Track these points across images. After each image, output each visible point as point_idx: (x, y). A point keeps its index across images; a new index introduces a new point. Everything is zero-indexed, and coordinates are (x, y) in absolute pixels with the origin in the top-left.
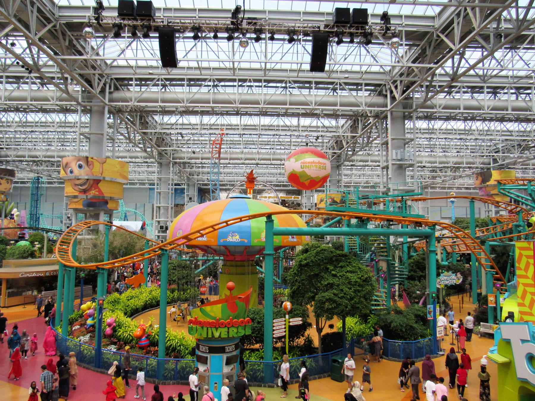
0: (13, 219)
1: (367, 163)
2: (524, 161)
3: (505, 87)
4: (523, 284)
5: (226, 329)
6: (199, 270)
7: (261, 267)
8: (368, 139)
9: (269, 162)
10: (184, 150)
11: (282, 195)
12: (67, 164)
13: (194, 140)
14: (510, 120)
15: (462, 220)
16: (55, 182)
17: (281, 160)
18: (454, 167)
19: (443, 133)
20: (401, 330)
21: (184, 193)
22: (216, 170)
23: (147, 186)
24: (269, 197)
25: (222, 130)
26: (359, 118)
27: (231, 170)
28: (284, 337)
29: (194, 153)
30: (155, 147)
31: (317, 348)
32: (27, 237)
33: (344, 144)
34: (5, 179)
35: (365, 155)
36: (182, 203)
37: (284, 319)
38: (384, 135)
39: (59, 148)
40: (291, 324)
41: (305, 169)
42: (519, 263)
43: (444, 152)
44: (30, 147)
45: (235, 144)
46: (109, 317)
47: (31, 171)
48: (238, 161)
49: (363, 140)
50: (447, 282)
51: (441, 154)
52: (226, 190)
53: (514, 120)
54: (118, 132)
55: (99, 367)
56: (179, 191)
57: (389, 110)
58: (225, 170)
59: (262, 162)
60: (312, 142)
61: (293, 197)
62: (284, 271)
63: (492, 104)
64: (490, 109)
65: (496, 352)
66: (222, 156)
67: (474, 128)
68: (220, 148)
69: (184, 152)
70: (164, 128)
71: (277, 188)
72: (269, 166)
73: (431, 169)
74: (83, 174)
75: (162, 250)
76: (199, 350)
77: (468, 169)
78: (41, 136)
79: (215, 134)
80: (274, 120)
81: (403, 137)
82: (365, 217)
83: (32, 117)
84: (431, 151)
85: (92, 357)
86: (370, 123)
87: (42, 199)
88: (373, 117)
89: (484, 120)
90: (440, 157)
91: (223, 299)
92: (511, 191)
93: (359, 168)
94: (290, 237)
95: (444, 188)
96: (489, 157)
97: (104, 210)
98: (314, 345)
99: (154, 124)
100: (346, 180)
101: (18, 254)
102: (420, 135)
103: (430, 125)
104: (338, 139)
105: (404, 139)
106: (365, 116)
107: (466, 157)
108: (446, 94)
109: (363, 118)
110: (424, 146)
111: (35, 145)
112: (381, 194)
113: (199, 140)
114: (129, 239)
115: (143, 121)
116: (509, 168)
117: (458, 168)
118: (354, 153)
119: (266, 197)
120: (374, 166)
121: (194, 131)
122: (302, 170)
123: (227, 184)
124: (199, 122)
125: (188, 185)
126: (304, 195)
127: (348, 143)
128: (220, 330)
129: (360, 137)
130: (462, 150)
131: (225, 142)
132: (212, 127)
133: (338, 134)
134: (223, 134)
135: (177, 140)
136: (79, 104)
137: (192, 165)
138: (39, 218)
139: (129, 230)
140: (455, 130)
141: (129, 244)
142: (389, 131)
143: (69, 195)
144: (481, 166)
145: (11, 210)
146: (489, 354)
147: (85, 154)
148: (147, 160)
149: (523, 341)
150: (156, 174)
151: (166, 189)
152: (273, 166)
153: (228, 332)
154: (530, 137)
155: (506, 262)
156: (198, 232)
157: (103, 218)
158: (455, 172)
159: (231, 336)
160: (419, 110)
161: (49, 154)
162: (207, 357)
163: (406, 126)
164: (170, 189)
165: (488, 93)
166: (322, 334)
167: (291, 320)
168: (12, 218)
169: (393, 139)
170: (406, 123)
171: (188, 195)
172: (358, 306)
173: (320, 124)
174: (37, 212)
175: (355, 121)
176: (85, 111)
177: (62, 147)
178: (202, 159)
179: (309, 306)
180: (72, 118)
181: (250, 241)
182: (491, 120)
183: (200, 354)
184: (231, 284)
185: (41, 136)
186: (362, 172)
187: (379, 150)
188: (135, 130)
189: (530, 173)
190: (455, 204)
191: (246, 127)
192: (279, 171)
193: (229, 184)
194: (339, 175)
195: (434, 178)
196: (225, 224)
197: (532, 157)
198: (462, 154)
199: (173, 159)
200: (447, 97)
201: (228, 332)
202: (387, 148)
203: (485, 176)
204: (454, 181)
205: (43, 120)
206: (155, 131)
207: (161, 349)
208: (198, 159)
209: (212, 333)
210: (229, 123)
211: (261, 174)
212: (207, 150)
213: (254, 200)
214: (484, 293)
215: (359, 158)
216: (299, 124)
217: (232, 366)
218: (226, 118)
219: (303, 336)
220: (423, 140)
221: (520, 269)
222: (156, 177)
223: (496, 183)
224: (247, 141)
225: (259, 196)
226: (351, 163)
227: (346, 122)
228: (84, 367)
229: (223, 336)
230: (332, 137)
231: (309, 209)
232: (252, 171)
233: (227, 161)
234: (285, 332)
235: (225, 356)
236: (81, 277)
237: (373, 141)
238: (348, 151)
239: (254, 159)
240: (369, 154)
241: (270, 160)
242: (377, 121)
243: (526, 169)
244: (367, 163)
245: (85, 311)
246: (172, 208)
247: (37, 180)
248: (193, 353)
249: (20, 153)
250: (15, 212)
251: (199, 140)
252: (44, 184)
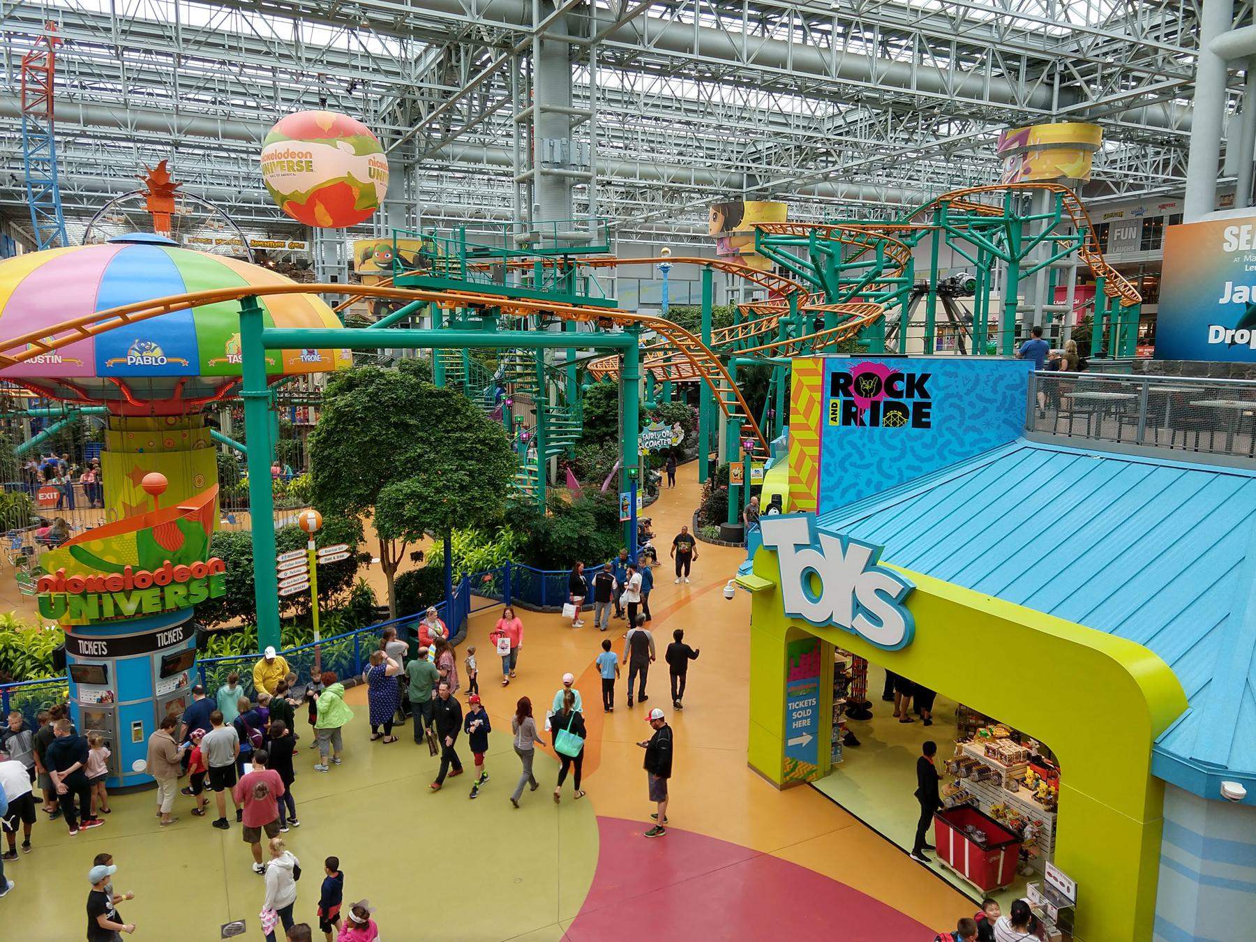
2: (806, 184)
3: (785, 9)
4: (800, 441)
5: (157, 591)
6: (24, 446)
8: (483, 106)
9: (212, 141)
11: (253, 236)
14: (786, 90)
17: (249, 139)
18: (671, 188)
20: (570, 548)
24: (219, 242)
25: (51, 25)
26: (461, 44)
27: (89, 155)
28: (307, 593)
31: (385, 608)
35: (473, 146)
37: (304, 552)
38: (524, 96)
40: (322, 561)
42: (796, 403)
43: (653, 150)
45: (100, 76)
49: (470, 106)
50: (655, 444)
51: (645, 156)
52: (79, 214)
53: (758, 86)
57: (537, 33)
58: (69, 153)
60: (336, 97)
61: (287, 242)
62: (281, 437)
63: (756, 47)
64: (654, 42)
65: (750, 572)
67: (716, 99)
68: (51, 84)
71: (239, 217)
72: (214, 153)
73: (623, 189)
79: (25, 36)
80: (222, 15)
81: (567, 109)
84: (626, 148)
86: (489, 60)
88: (496, 46)
89: (737, 84)
92: (780, 249)
93: (457, 175)
94: (305, 351)
95: (648, 236)
96: (740, 171)
98: (376, 602)
100: (426, 206)
102: (604, 107)
103: (626, 80)
104: (407, 96)
105: (570, 114)
106: (472, 38)
107: (698, 166)
108: (663, 9)
112: (515, 248)
116: (776, 198)
117: (678, 191)
119: (209, 241)
122: (368, 180)
123: (81, 198)
126: (319, 240)
127: (432, 107)
128: (136, 596)
129: (463, 95)
131: (64, 67)
133: (407, 82)
144: (725, 189)
146: (739, 577)
149: (798, 547)
152: (225, 154)
154: (820, 132)
155: (763, 398)
156: (33, 339)
158: (672, 199)
160: (604, 42)
162: (105, 667)
165: (751, 19)
166: (396, 575)
167: (322, 552)
170: (574, 70)
173: (355, 46)
179: (361, 517)
181: (195, 363)
182: (751, 85)
183: (80, 661)
184: (154, 477)
186: (466, 187)
187: (508, 135)
189: (813, 211)
193: (89, 198)
194: (410, 190)
195: (628, 211)
197: (820, 176)
198: (687, 159)
200: (667, 17)
201: (162, 598)
202: (531, 131)
203: (731, 213)
209: (116, 605)
211: (190, 174)
213: (257, 266)
214: (721, 462)
215: (459, 150)
217: (180, 677)
219: (349, 584)
220: (609, 117)
221: (797, 412)
223: (753, 229)
224: (140, 71)
226: (439, 162)
227: (425, 51)
229: (147, 608)
230: (389, 89)
231: (334, 279)
232: (163, 164)
234: (309, 580)
235: (157, 657)
237: (494, 109)
239: (165, 129)
240: (483, 144)
243: (806, 201)
248: (58, 660)
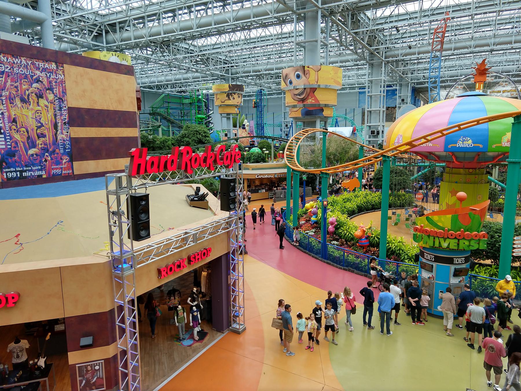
7: (491, 175)
9: (509, 46)
10: (397, 46)
12: (286, 76)
13: (411, 32)
16: (274, 93)
21: (396, 94)
22: (437, 65)
23: (357, 90)
25: (447, 13)
29: (410, 47)
30: (366, 47)
32: (256, 144)
34: (237, 94)
36: (394, 106)
39: (276, 60)
44: (254, 62)
46: (332, 217)
47: (256, 84)
48: (466, 50)
52: (445, 87)
55: (325, 259)
56: (391, 93)
58: (446, 63)
66: (445, 46)
68: (443, 37)
69: (398, 49)
71: (516, 79)
72: (508, 51)
74: (300, 84)
75: (384, 156)
76: (423, 256)
78: (262, 51)
79: (437, 20)
83: (254, 33)
85: (319, 249)
87: (265, 109)
99: (367, 21)
101: (254, 159)
111: (257, 60)
113: (416, 31)
114: (344, 145)
115: (355, 20)
119: (499, 92)
125: (401, 85)
128: (448, 241)
134: (448, 19)
135: (391, 35)
136: (294, 12)
139: (343, 136)
141: (343, 149)
145: (243, 121)
147: (302, 63)
148: (358, 62)
150: (366, 77)
151: (378, 91)
152: (514, 51)
153: (458, 244)
157: (319, 125)
159: (461, 247)
161: (269, 67)
164: (382, 92)
171: (400, 97)
174: (261, 122)
176: (299, 20)
178: (419, 54)
180: (288, 28)
184: (461, 194)
185: (262, 51)
188: (346, 31)
193: (450, 80)
196: (457, 128)
199: (386, 58)
201: (458, 244)
205: (263, 34)
206: (367, 29)
207: (382, 252)
208: (414, 54)
209: (440, 243)
210: (457, 3)
211: (495, 63)
217: (461, 278)
222: (367, 79)
228: (313, 257)
229: (451, 247)
232: (484, 60)
233: (450, 52)
235: (453, 268)
241: (510, 43)
248: (416, 258)
250: (246, 122)
251: (416, 31)
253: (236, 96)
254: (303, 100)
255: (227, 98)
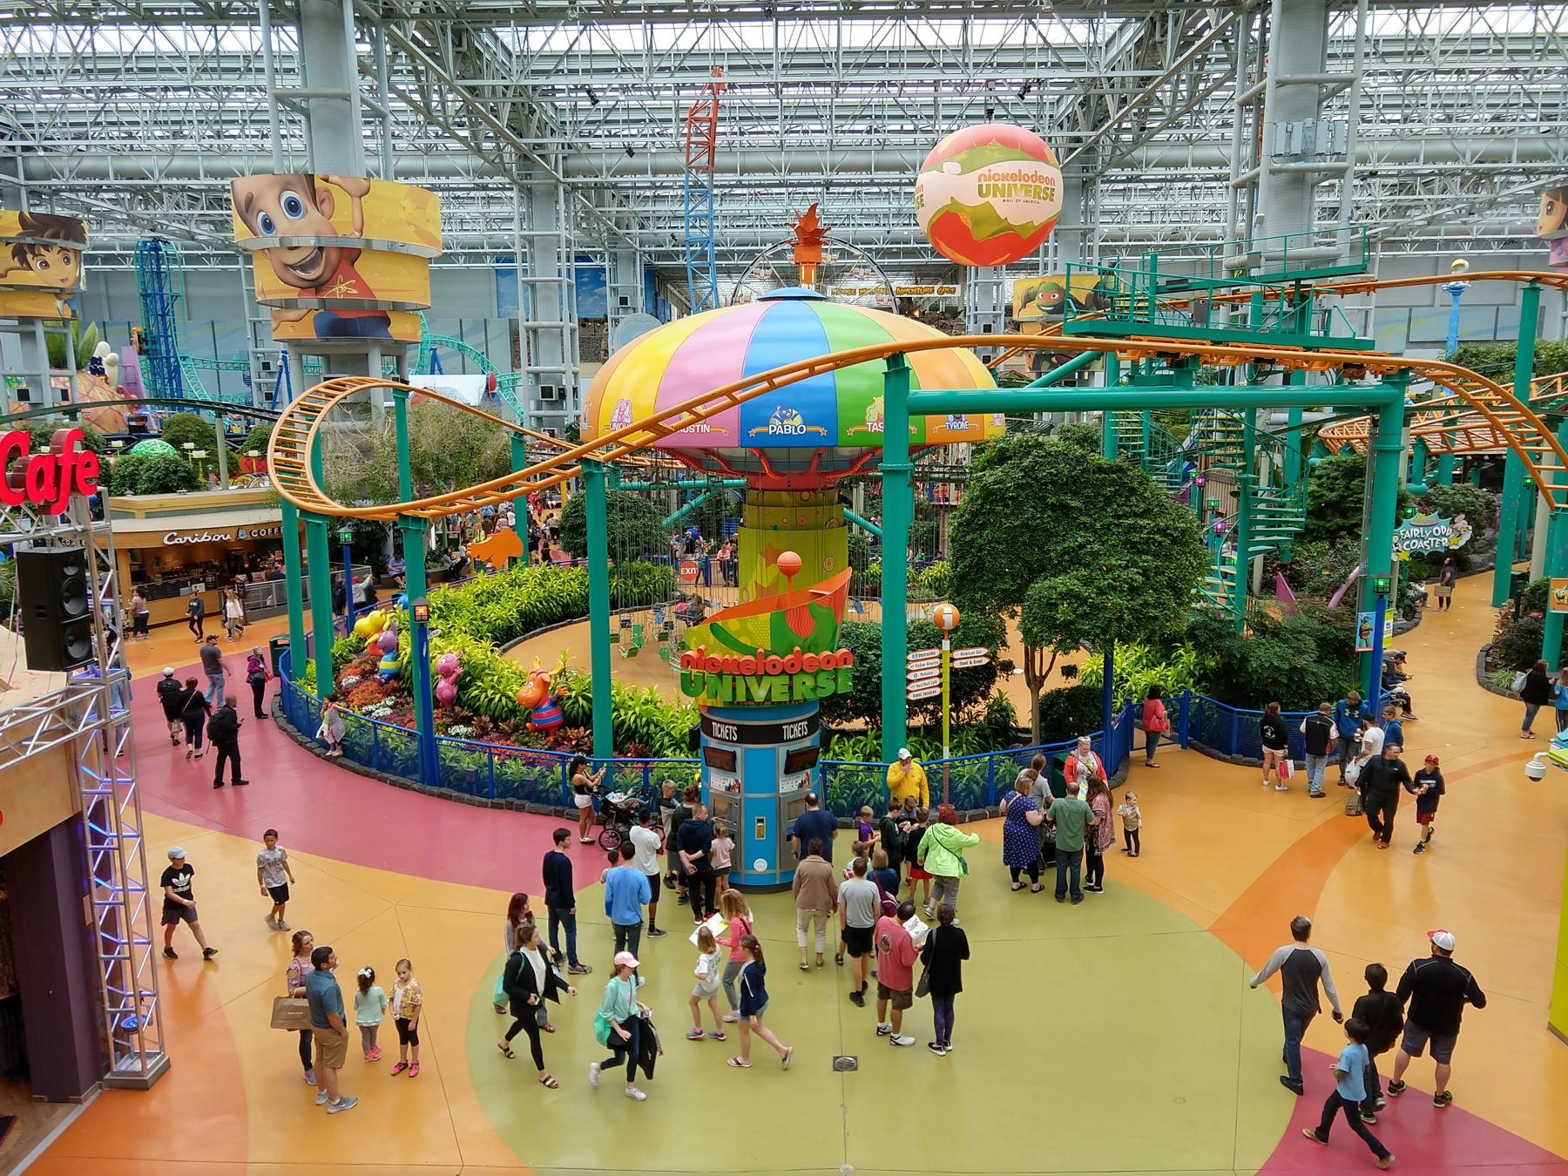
0: (101, 372)
1: (1180, 171)
8: (1192, 90)
11: (901, 282)
12: (250, 201)
13: (628, 109)
15: (1482, 348)
18: (1475, 172)
19: (1456, 52)
25: (717, 71)
26: (1170, 12)
28: (937, 700)
29: (630, 152)
30: (507, 137)
31: (1027, 731)
32: (154, 428)
33: (1111, 105)
34: (56, 249)
36: (601, 317)
37: (937, 652)
38: (1254, 68)
40: (957, 665)
41: (990, 199)
44: (117, 143)
47: (133, 220)
52: (728, 271)
54: (392, 89)
56: (590, 280)
58: (725, 206)
59: (844, 176)
60: (1004, 105)
61: (937, 287)
68: (713, 134)
69: (598, 152)
70: (534, 72)
71: (886, 261)
72: (865, 189)
73: (1395, 181)
74: (304, 231)
75: (587, 462)
77: (1523, 178)
79: (693, 86)
82: (1187, 350)
87: (179, 308)
90: (1432, 137)
91: (748, 604)
93: (1151, 186)
94: (951, 417)
95: (1432, 245)
97: (379, 343)
98: (1015, 722)
99: (502, 57)
100: (1106, 229)
101: (151, 480)
103: (1413, 22)
105: (1320, 83)
109: (1183, 12)
110: (1383, 102)
112: (1224, 276)
114: (463, 430)
117: (1489, 174)
118: (1143, 135)
120: (1204, 180)
121: (628, 79)
122: (983, 201)
123: (732, 253)
124: (640, 45)
125: (615, 258)
127: (1124, 101)
128: (766, 681)
129: (1166, 80)
130: (1512, 110)
131: (726, 114)
132: (685, 61)
135: (574, 110)
137: (624, 193)
138: (177, 368)
139: (457, 401)
140: (1498, 39)
142: (1270, 55)
143: (269, 297)
148: (486, 180)
150: (515, 225)
151: (553, 271)
152: (876, 189)
153: (791, 688)
156: (689, 408)
157: (378, 368)
161: (178, 163)
162: (734, 753)
163: (1331, 30)
164: (564, 273)
166: (1042, 692)
167: (957, 654)
168: (98, 371)
169: (1281, 84)
170: (1331, 19)
171: (615, 290)
172: (1153, 612)
175: (1153, 21)
177: (215, 142)
178: (655, 173)
181: (834, 432)
183: (713, 744)
184: (789, 557)
186: (1162, 201)
188: (440, 78)
190: (1463, 298)
191: (796, 61)
192: (895, 204)
193: (739, 253)
196: (765, 385)
198: (1508, 125)
199: (567, 174)
201: (791, 688)
204: (1471, 219)
207: (601, 736)
208: (644, 171)
209: (748, 689)
211: (838, 216)
212: (667, 141)
215: (1155, 153)
216: (965, 44)
217: (802, 776)
218: (729, 31)
219: (985, 697)
222: (517, 233)
225: (830, 288)
226: (1128, 171)
227: (1121, 29)
229: (776, 698)
230: (1070, 85)
232: (813, 208)
233: (732, 178)
234: (940, 685)
235: (782, 750)
236: (342, 540)
237: (1208, 91)
238: (1120, 130)
239: (818, 169)
240: (1190, 141)
241: (867, 169)
242: (1232, 22)
244: (1180, 171)
245: (369, 636)
246: (572, 331)
247: (153, 249)
249: (87, 164)
250: (102, 350)
252: (175, 261)
253: (52, 256)
254: (317, 286)
255: (16, 263)
